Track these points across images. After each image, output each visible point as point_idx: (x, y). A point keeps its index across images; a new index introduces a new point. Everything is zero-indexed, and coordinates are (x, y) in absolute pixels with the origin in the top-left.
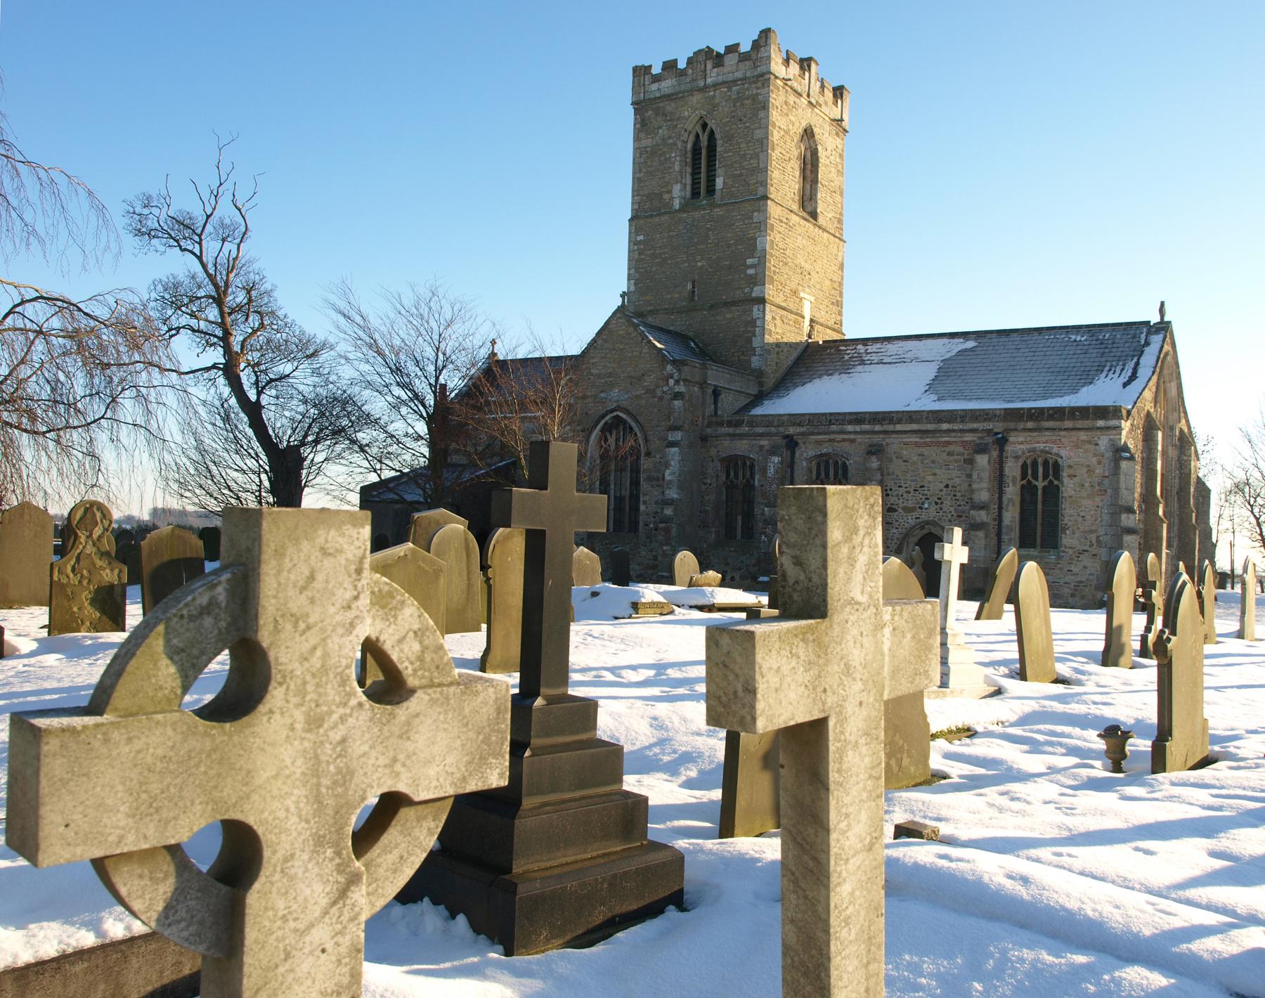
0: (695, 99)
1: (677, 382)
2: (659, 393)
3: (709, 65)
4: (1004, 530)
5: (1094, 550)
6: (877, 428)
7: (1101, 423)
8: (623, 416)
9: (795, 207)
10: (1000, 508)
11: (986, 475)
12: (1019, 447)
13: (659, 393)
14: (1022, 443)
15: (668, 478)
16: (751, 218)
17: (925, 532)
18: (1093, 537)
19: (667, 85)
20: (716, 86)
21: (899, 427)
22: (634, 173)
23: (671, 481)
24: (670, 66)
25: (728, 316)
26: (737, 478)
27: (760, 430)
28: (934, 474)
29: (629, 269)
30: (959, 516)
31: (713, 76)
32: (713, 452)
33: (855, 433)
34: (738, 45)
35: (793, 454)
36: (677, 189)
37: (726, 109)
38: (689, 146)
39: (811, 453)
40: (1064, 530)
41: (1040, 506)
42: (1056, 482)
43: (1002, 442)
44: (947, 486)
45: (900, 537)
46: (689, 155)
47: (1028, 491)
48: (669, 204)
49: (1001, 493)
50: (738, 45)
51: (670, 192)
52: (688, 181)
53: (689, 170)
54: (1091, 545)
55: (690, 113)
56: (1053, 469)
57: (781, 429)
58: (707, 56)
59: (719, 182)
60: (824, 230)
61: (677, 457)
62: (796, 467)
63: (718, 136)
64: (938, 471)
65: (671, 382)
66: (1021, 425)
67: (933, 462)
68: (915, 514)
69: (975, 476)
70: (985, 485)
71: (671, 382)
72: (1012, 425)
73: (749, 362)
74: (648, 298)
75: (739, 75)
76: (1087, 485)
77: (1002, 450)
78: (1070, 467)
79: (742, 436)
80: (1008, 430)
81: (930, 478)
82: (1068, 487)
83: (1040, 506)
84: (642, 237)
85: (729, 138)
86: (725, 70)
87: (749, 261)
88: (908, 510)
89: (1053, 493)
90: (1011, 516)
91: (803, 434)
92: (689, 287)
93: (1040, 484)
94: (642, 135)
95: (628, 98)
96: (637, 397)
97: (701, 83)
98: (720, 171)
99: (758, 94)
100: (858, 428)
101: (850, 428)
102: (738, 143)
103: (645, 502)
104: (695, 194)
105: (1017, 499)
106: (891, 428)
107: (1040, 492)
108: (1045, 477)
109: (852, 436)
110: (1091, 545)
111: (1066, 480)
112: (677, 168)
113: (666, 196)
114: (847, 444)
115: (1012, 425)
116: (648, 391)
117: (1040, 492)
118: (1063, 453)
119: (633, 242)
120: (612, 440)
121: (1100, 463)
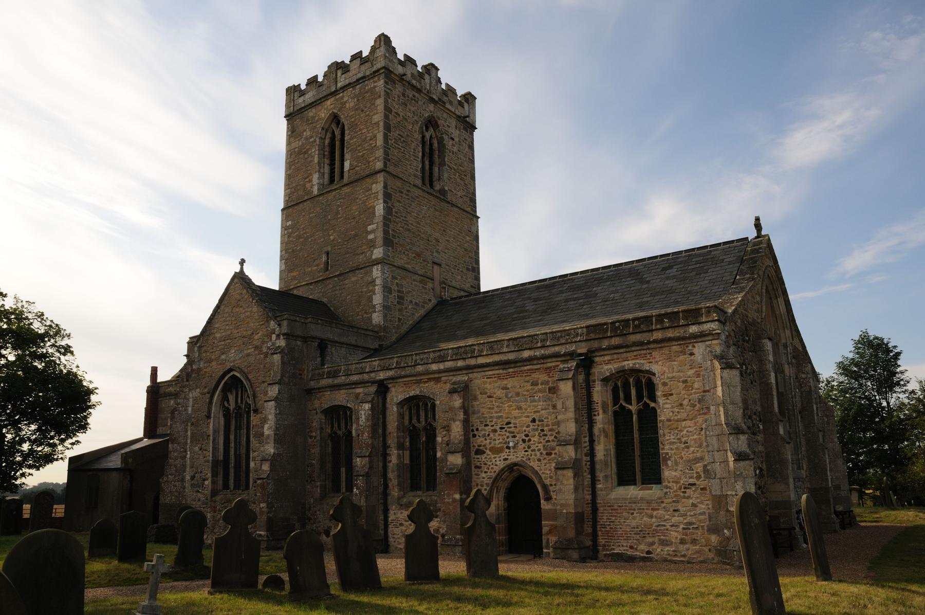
0: (329, 102)
1: (278, 336)
2: (264, 350)
3: (339, 72)
4: (598, 466)
5: (702, 483)
6: (460, 363)
7: (694, 329)
8: (238, 375)
9: (419, 182)
10: (592, 441)
11: (571, 403)
12: (606, 367)
13: (264, 350)
14: (609, 362)
15: (266, 432)
16: (371, 189)
17: (515, 474)
18: (699, 467)
19: (309, 98)
20: (344, 88)
21: (481, 361)
22: (286, 171)
23: (269, 435)
24: (313, 81)
25: (353, 279)
26: (340, 429)
27: (355, 378)
28: (520, 408)
29: (281, 251)
30: (549, 454)
31: (342, 81)
32: (317, 404)
33: (440, 372)
34: (361, 52)
35: (385, 399)
36: (315, 178)
37: (352, 104)
38: (327, 141)
39: (401, 397)
40: (666, 460)
41: (636, 435)
42: (652, 405)
43: (586, 363)
44: (534, 421)
45: (490, 482)
46: (327, 149)
47: (621, 418)
48: (311, 192)
49: (591, 423)
50: (361, 52)
51: (311, 181)
52: (327, 169)
53: (327, 161)
54: (699, 477)
55: (323, 113)
56: (645, 385)
57: (373, 375)
58: (337, 67)
59: (347, 165)
60: (453, 205)
61: (273, 411)
62: (388, 414)
63: (346, 128)
64: (523, 405)
65: (274, 337)
66: (605, 344)
67: (518, 394)
68: (504, 455)
69: (559, 406)
70: (571, 414)
71: (274, 337)
72: (596, 344)
73: (370, 319)
74: (294, 274)
75: (360, 75)
76: (685, 402)
77: (588, 375)
78: (665, 384)
79: (339, 387)
80: (590, 351)
81: (516, 413)
82: (665, 409)
83: (636, 435)
84: (290, 223)
85: (354, 126)
86: (350, 74)
87: (370, 228)
88: (496, 451)
89: (649, 417)
90: (604, 449)
91: (392, 378)
92: (324, 258)
93: (633, 408)
94: (292, 139)
95: (282, 111)
96: (248, 355)
97: (333, 89)
98: (347, 156)
99: (375, 87)
100: (442, 366)
101: (434, 367)
102: (360, 130)
103: (254, 459)
104: (332, 180)
105: (611, 429)
106: (472, 362)
107: (635, 417)
108: (640, 398)
109: (437, 376)
110: (699, 477)
111: (661, 400)
112: (316, 160)
113: (308, 185)
114: (432, 383)
115: (596, 344)
116: (256, 348)
117: (635, 417)
118: (655, 368)
119: (284, 228)
120: (231, 398)
121: (698, 376)
